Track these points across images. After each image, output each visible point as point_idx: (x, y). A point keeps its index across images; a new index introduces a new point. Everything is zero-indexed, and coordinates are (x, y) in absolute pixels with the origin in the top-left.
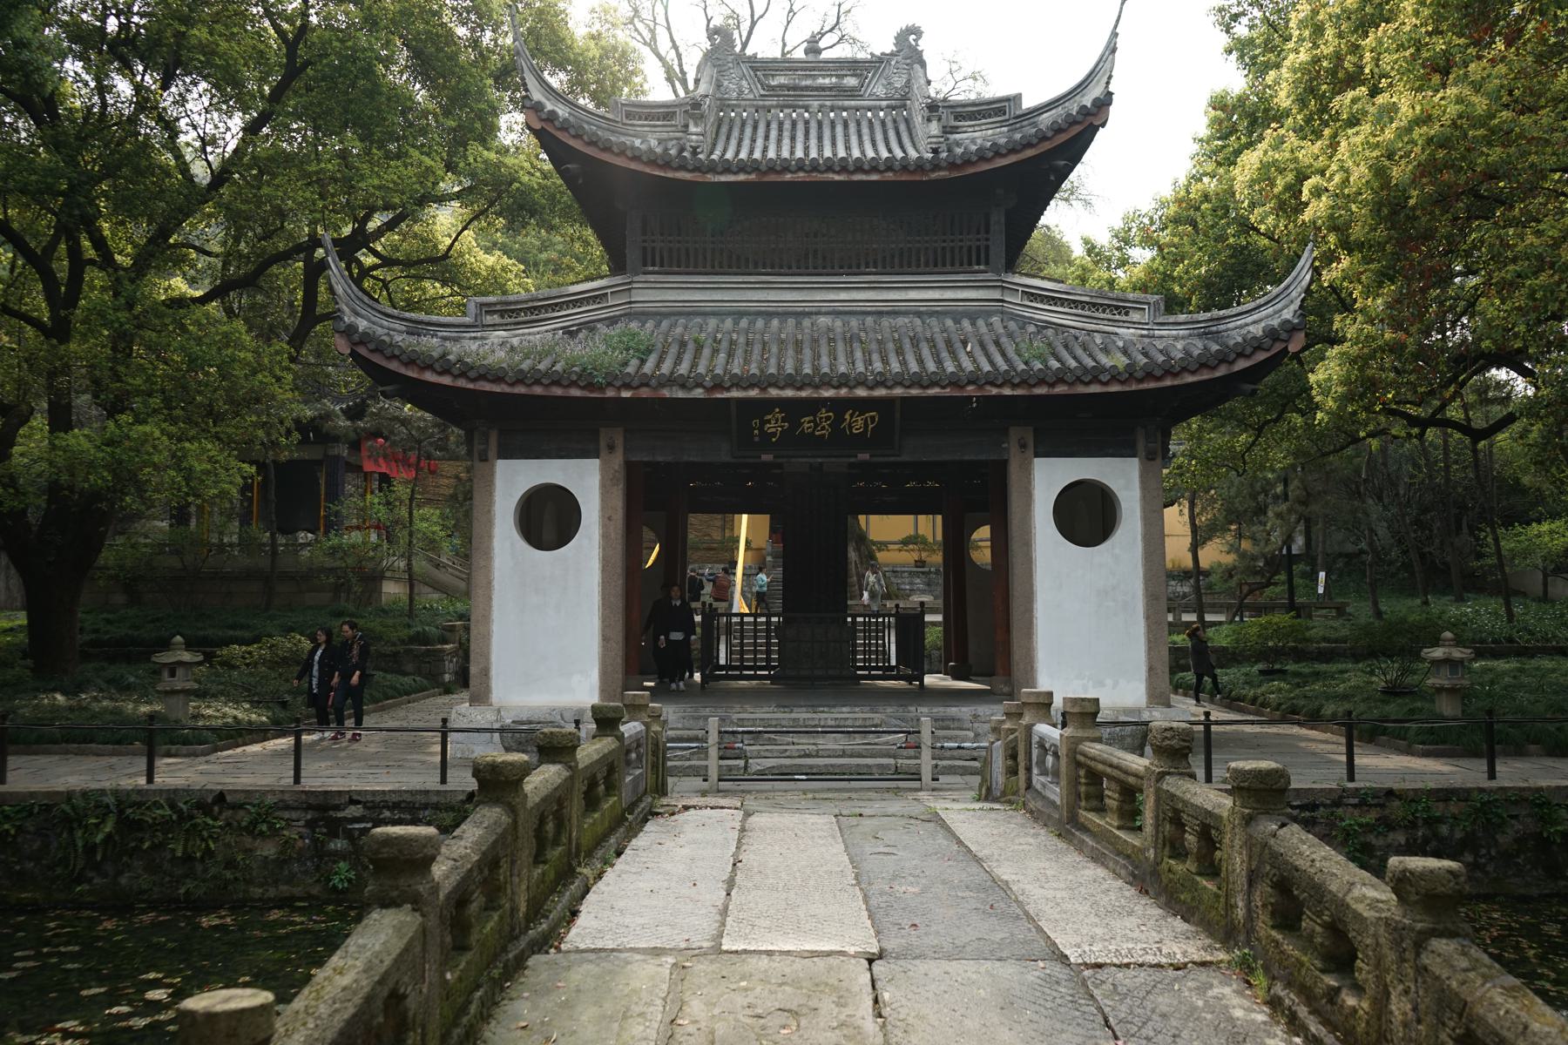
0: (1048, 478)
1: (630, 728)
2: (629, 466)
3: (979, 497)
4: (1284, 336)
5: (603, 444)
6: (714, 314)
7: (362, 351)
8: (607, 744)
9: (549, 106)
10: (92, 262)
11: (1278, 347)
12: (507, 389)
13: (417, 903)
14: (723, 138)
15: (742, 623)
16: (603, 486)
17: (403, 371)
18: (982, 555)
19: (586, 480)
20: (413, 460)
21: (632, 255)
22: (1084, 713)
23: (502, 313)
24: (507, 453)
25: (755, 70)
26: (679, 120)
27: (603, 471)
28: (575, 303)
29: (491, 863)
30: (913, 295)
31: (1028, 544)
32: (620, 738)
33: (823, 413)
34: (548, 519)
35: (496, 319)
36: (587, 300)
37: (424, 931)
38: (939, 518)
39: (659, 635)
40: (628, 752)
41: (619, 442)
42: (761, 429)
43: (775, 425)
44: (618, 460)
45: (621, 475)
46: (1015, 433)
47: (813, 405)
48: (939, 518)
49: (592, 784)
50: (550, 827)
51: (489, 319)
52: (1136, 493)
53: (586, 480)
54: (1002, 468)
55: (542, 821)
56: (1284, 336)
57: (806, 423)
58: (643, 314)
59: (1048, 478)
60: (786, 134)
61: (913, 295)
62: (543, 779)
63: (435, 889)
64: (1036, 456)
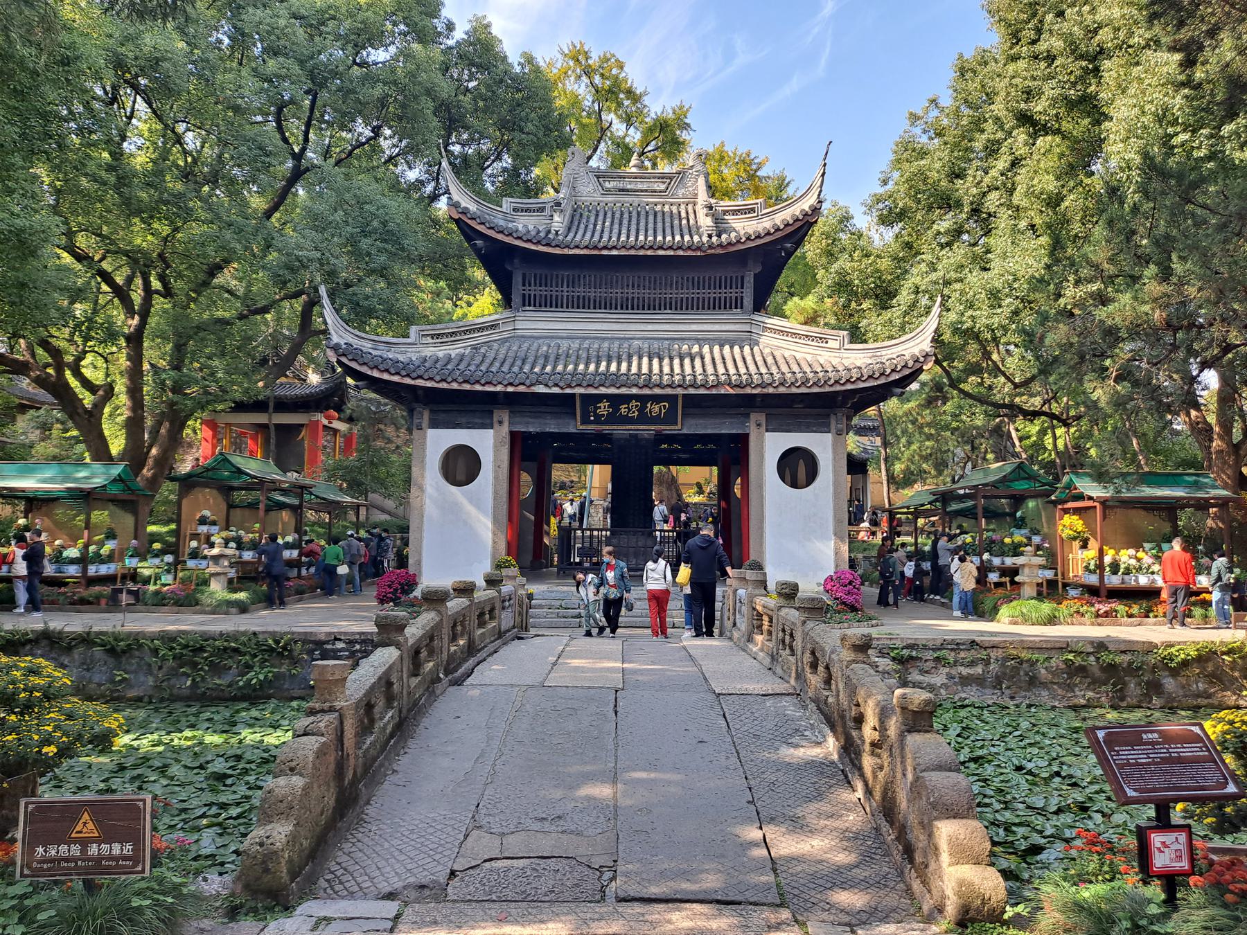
0: (771, 446)
1: (506, 588)
2: (513, 434)
3: (732, 457)
4: (922, 359)
5: (495, 419)
6: (568, 338)
7: (344, 360)
8: (492, 593)
9: (463, 204)
10: (157, 292)
11: (918, 366)
12: (436, 385)
13: (398, 646)
14: (574, 228)
15: (591, 537)
16: (495, 446)
17: (369, 372)
18: (737, 491)
19: (488, 443)
20: (137, 297)
21: (516, 299)
22: (789, 592)
23: (432, 336)
24: (434, 424)
25: (598, 177)
26: (547, 212)
27: (495, 437)
28: (480, 330)
29: (431, 636)
30: (694, 327)
31: (761, 486)
32: (499, 592)
33: (634, 403)
34: (461, 467)
35: (429, 340)
36: (487, 328)
37: (401, 657)
38: (715, 469)
39: (535, 543)
40: (503, 601)
41: (506, 419)
42: (595, 412)
43: (604, 408)
44: (505, 430)
45: (507, 440)
46: (753, 416)
47: (627, 398)
48: (715, 469)
49: (481, 615)
50: (459, 628)
51: (424, 340)
52: (830, 455)
53: (488, 443)
54: (745, 437)
55: (455, 625)
56: (922, 359)
57: (623, 409)
58: (523, 337)
59: (771, 446)
60: (616, 221)
61: (694, 327)
62: (455, 605)
63: (406, 640)
64: (767, 431)
